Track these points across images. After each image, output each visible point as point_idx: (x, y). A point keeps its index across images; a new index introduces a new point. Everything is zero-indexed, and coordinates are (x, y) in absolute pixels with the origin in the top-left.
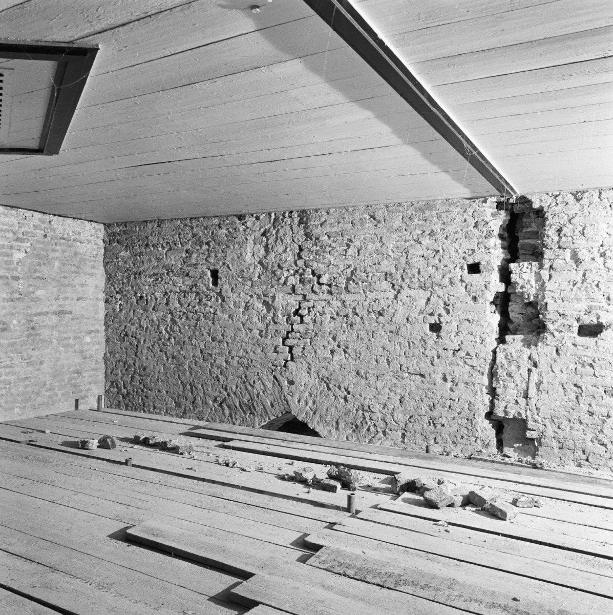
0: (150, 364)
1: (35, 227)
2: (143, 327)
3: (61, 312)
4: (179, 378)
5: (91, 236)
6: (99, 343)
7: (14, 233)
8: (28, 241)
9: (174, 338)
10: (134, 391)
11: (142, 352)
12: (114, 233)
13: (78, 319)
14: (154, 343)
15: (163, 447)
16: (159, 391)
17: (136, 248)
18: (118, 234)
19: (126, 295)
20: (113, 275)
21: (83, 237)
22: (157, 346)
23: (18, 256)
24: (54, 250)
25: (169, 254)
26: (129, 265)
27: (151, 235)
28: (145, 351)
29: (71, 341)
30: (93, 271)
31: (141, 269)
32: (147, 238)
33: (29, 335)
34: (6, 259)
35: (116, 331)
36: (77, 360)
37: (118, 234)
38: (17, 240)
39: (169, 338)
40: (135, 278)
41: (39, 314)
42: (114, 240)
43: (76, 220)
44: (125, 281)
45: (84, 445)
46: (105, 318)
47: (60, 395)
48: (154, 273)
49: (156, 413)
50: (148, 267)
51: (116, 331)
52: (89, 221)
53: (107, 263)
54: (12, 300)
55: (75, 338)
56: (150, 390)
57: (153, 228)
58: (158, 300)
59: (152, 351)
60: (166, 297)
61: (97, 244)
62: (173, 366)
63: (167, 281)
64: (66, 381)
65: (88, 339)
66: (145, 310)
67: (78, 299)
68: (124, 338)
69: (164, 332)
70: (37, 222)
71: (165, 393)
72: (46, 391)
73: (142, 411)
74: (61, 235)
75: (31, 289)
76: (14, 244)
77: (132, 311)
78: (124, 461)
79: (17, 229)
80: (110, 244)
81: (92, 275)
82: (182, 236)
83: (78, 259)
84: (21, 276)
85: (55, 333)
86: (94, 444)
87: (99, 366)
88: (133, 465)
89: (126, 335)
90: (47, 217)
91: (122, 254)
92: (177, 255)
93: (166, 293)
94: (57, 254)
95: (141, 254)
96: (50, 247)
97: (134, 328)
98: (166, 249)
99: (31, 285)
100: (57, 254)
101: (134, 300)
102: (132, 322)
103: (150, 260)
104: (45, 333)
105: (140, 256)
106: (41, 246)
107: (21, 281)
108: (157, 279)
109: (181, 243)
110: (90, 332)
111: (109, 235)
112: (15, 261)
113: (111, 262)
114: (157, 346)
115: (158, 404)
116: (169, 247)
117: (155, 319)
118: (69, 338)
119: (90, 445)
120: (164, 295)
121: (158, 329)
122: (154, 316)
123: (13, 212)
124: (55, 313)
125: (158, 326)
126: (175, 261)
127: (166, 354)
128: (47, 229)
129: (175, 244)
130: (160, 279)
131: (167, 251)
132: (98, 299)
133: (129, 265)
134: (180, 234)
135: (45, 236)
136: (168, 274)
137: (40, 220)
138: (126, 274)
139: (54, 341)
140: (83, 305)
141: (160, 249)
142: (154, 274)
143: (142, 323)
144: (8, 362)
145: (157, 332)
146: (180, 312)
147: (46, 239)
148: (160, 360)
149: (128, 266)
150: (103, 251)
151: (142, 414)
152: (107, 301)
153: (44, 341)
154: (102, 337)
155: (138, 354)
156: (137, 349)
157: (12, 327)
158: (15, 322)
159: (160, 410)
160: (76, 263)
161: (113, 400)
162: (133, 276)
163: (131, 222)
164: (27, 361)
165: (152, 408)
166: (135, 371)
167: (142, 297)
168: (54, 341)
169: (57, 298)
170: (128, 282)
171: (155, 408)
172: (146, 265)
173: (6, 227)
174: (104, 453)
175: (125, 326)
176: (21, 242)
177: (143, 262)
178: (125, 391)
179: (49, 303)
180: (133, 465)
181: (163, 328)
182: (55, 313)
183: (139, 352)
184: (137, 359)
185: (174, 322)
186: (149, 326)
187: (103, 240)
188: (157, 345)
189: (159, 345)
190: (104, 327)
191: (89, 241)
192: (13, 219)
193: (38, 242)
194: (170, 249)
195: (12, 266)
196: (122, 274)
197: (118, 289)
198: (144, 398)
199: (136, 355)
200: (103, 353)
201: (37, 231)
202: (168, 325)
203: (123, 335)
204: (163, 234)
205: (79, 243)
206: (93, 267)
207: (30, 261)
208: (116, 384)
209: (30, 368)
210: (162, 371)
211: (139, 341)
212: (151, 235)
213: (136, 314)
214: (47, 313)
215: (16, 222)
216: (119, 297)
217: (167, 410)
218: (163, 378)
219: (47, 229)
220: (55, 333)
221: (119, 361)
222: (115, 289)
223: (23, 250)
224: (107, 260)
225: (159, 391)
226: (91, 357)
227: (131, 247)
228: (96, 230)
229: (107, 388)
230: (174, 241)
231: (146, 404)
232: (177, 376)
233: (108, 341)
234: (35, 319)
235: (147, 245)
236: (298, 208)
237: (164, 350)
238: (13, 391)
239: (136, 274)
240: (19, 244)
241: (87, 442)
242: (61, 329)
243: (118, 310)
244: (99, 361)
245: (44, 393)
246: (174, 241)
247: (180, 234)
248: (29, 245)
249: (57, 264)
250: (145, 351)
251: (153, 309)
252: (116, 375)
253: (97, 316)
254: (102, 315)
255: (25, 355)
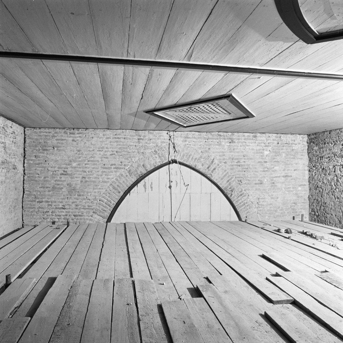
0: (328, 201)
1: (273, 140)
2: (324, 183)
3: (286, 176)
4: (340, 208)
5: (300, 141)
6: (305, 190)
7: (264, 144)
8: (270, 146)
9: (338, 189)
10: (321, 214)
11: (324, 195)
12: (311, 138)
13: (294, 179)
14: (329, 191)
15: (311, 236)
16: (332, 215)
17: (320, 145)
18: (313, 139)
19: (317, 168)
20: (312, 158)
21: (296, 142)
22: (330, 193)
23: (266, 153)
24: (282, 149)
25: (334, 147)
26: (318, 153)
27: (327, 138)
28: (325, 195)
29: (291, 189)
30: (302, 157)
31: (323, 155)
32: (325, 139)
33: (272, 186)
34: (261, 154)
35: (314, 185)
36: (294, 198)
37: (313, 139)
38: (266, 146)
39: (336, 188)
40: (321, 159)
41: (276, 177)
42: (311, 141)
43: (293, 135)
44: (316, 161)
45: (279, 231)
46: (309, 179)
47: (286, 213)
48: (328, 157)
49: (331, 226)
50: (326, 154)
51: (314, 185)
52: (299, 134)
53: (309, 153)
54: (264, 171)
55: (293, 188)
56: (328, 214)
57: (327, 134)
58: (331, 170)
59: (328, 195)
60: (334, 168)
61: (304, 145)
62: (338, 203)
63: (334, 160)
64: (289, 207)
65: (300, 188)
66: (325, 175)
67: (294, 170)
68: (316, 188)
69: (333, 185)
70: (274, 138)
71: (334, 216)
72: (280, 210)
73: (325, 224)
74: (286, 142)
75: (272, 166)
76: (264, 148)
77: (320, 176)
78: (288, 237)
79: (266, 141)
80: (310, 144)
81: (301, 159)
82: (340, 137)
83: (294, 152)
84: (268, 161)
85: (284, 186)
86: (283, 230)
87: (306, 201)
88: (292, 240)
89: (318, 187)
90: (279, 135)
91: (314, 148)
92: (338, 147)
93: (334, 166)
94: (284, 151)
95: (322, 148)
96: (281, 148)
97: (320, 184)
98: (333, 144)
99: (272, 165)
100: (284, 151)
101: (321, 170)
102: (320, 180)
103: (326, 150)
104: (279, 185)
105: (322, 149)
106: (277, 148)
107: (268, 163)
108: (330, 160)
109: (339, 141)
110: (300, 186)
111: (310, 140)
112: (265, 155)
113: (311, 152)
114: (330, 193)
115: (332, 222)
116: (334, 143)
117: (330, 179)
118: (290, 188)
119: (281, 231)
120: (333, 167)
121: (331, 184)
122: (329, 178)
123: (264, 135)
124: (283, 177)
125: (331, 182)
126: (337, 150)
127: (334, 196)
128: (279, 140)
129: (337, 142)
130: (331, 159)
131: (334, 145)
132: (305, 170)
133: (318, 153)
134: (339, 136)
135: (278, 143)
136: (334, 157)
137: (275, 137)
138: (317, 158)
139: (283, 189)
140: (297, 173)
141: (330, 144)
142: (329, 157)
143: (324, 181)
144: (263, 197)
145: (330, 186)
146: (340, 175)
147: (278, 145)
148: (332, 200)
149: (317, 154)
150: (307, 147)
151: (324, 226)
152: (309, 171)
153: (279, 189)
154: (307, 188)
155: (323, 196)
156: (322, 194)
157: (264, 182)
158: (266, 180)
159: (332, 224)
160: (293, 154)
161: (313, 218)
162: (319, 159)
163: (318, 133)
164: (271, 197)
165: (329, 223)
166: (321, 205)
167: (324, 169)
168: (283, 189)
169: (284, 170)
170: (318, 162)
171: (330, 223)
172: (325, 153)
173: (261, 141)
174: (287, 235)
175: (317, 183)
176: (268, 147)
177: (323, 151)
178: (317, 214)
179: (281, 172)
180: (292, 240)
181: (333, 184)
182: (283, 177)
183: (323, 195)
184: (322, 198)
185: (338, 181)
186: (327, 182)
187: (307, 142)
188: (330, 192)
189: (331, 192)
190: (308, 183)
191: (299, 143)
192: (264, 138)
193: (275, 146)
194: (335, 144)
195: (263, 157)
196: (315, 158)
197: (314, 165)
198: (325, 218)
199: (322, 197)
200: (308, 195)
201: (274, 142)
202: (335, 182)
203: (316, 187)
204: (331, 137)
205: (294, 145)
206: (302, 155)
207: (271, 154)
208: (314, 210)
209: (272, 200)
210: (333, 205)
211: (323, 190)
212: (327, 138)
213: (321, 177)
214: (279, 177)
215: (265, 139)
216: (314, 169)
217: (335, 224)
218: (333, 209)
219: (279, 140)
220: (284, 186)
221: (315, 199)
222: (312, 165)
223: (268, 150)
224: (309, 151)
225: (332, 215)
226: (301, 197)
227: (318, 144)
228: (303, 138)
229: (310, 212)
230: (336, 140)
231: (326, 221)
232: (339, 207)
233: (310, 189)
234: (274, 179)
235: (325, 143)
236: (312, 133)
237: (334, 194)
238: (265, 209)
239: (321, 157)
240: (267, 148)
241: (280, 229)
242: (287, 183)
243: (314, 175)
244: (306, 199)
245: (279, 211)
246: (336, 140)
247: (339, 136)
248: (271, 148)
249: (284, 155)
250: (325, 195)
251: (329, 174)
252: (314, 206)
253: (304, 178)
254: (307, 177)
255: (270, 194)
